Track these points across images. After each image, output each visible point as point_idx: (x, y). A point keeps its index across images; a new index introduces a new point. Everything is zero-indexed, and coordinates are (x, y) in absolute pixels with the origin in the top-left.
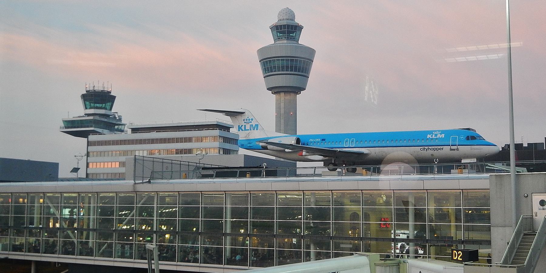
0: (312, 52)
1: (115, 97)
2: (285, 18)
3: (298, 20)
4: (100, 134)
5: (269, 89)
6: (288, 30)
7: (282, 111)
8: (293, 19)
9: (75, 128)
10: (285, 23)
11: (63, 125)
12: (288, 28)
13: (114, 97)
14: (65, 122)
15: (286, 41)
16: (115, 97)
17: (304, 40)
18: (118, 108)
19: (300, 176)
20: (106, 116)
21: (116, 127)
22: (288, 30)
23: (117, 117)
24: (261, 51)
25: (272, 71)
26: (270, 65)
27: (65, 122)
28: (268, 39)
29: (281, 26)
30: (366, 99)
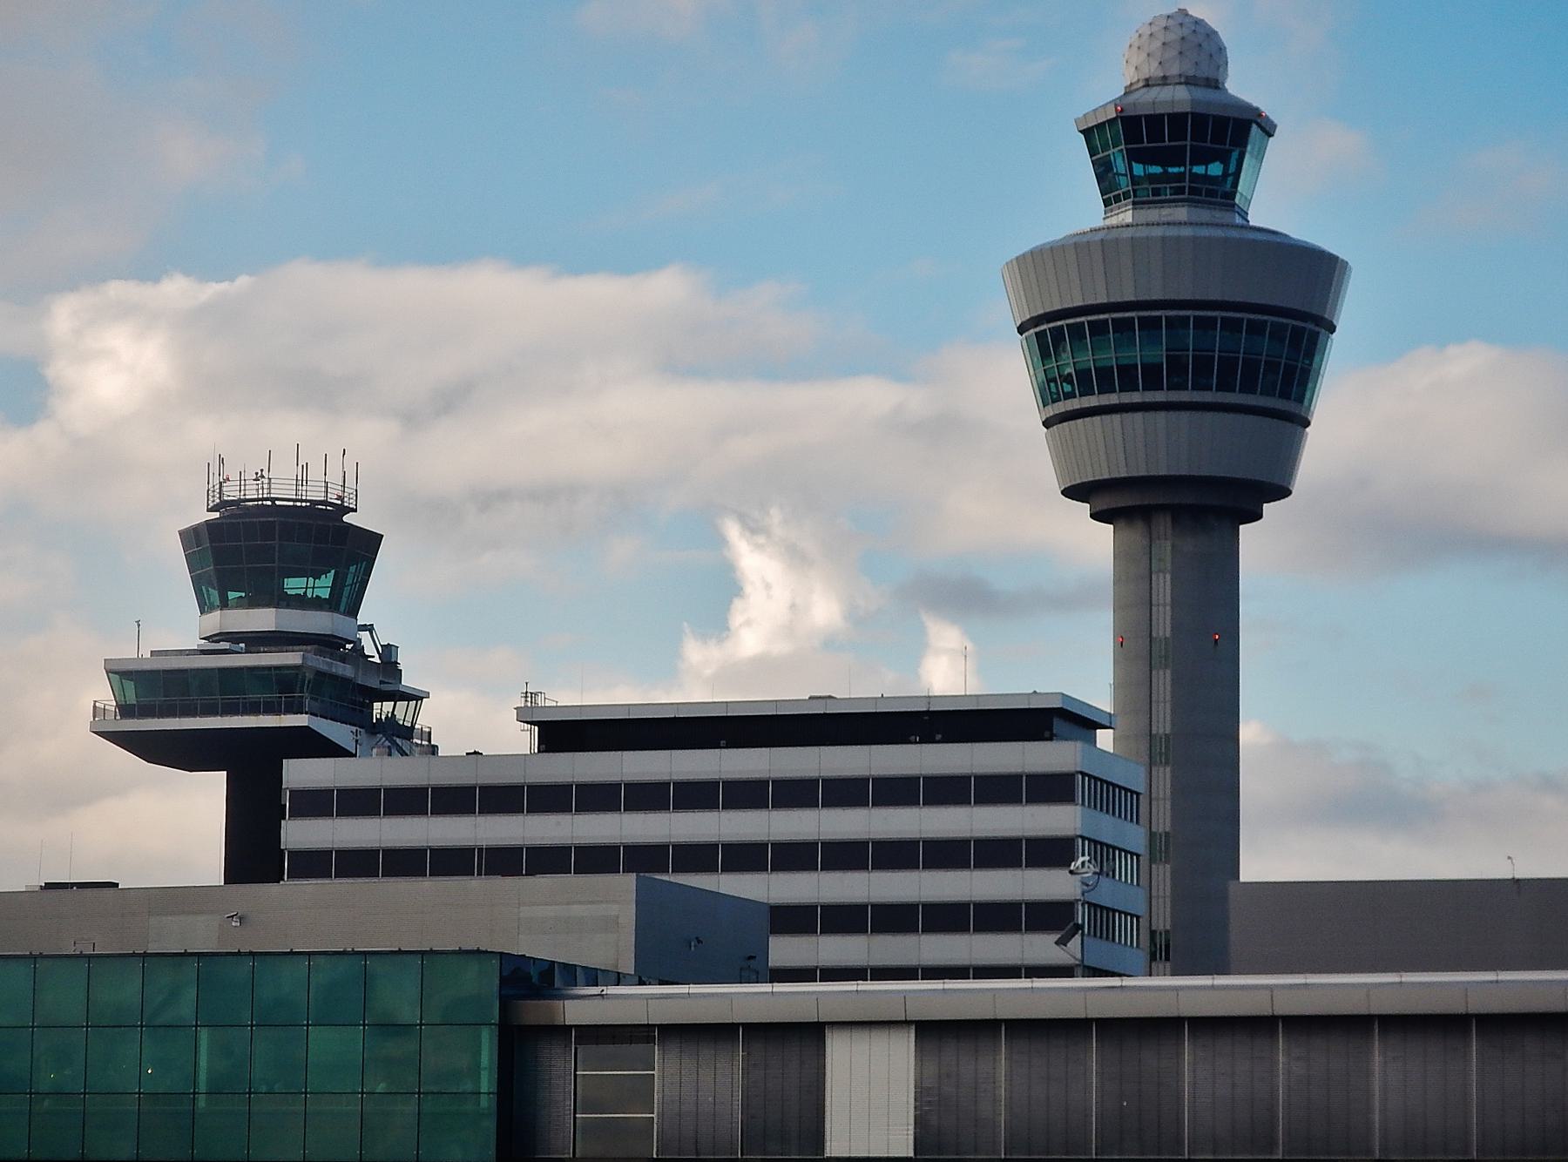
0: (1318, 271)
1: (375, 539)
2: (1174, 70)
3: (1243, 84)
4: (330, 750)
5: (1071, 492)
6: (1179, 142)
7: (1163, 628)
8: (1215, 84)
9: (160, 715)
10: (1178, 98)
11: (104, 695)
12: (1198, 134)
13: (372, 541)
14: (120, 674)
15: (1181, 213)
16: (375, 539)
17: (1280, 195)
18: (388, 611)
19: (313, 864)
20: (329, 644)
21: (382, 709)
22: (1179, 142)
23: (369, 650)
24: (1036, 265)
25: (1248, 388)
26: (1092, 349)
27: (120, 674)
28: (1074, 204)
29: (1154, 121)
30: (217, 515)
